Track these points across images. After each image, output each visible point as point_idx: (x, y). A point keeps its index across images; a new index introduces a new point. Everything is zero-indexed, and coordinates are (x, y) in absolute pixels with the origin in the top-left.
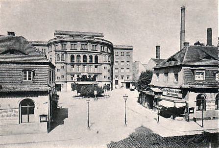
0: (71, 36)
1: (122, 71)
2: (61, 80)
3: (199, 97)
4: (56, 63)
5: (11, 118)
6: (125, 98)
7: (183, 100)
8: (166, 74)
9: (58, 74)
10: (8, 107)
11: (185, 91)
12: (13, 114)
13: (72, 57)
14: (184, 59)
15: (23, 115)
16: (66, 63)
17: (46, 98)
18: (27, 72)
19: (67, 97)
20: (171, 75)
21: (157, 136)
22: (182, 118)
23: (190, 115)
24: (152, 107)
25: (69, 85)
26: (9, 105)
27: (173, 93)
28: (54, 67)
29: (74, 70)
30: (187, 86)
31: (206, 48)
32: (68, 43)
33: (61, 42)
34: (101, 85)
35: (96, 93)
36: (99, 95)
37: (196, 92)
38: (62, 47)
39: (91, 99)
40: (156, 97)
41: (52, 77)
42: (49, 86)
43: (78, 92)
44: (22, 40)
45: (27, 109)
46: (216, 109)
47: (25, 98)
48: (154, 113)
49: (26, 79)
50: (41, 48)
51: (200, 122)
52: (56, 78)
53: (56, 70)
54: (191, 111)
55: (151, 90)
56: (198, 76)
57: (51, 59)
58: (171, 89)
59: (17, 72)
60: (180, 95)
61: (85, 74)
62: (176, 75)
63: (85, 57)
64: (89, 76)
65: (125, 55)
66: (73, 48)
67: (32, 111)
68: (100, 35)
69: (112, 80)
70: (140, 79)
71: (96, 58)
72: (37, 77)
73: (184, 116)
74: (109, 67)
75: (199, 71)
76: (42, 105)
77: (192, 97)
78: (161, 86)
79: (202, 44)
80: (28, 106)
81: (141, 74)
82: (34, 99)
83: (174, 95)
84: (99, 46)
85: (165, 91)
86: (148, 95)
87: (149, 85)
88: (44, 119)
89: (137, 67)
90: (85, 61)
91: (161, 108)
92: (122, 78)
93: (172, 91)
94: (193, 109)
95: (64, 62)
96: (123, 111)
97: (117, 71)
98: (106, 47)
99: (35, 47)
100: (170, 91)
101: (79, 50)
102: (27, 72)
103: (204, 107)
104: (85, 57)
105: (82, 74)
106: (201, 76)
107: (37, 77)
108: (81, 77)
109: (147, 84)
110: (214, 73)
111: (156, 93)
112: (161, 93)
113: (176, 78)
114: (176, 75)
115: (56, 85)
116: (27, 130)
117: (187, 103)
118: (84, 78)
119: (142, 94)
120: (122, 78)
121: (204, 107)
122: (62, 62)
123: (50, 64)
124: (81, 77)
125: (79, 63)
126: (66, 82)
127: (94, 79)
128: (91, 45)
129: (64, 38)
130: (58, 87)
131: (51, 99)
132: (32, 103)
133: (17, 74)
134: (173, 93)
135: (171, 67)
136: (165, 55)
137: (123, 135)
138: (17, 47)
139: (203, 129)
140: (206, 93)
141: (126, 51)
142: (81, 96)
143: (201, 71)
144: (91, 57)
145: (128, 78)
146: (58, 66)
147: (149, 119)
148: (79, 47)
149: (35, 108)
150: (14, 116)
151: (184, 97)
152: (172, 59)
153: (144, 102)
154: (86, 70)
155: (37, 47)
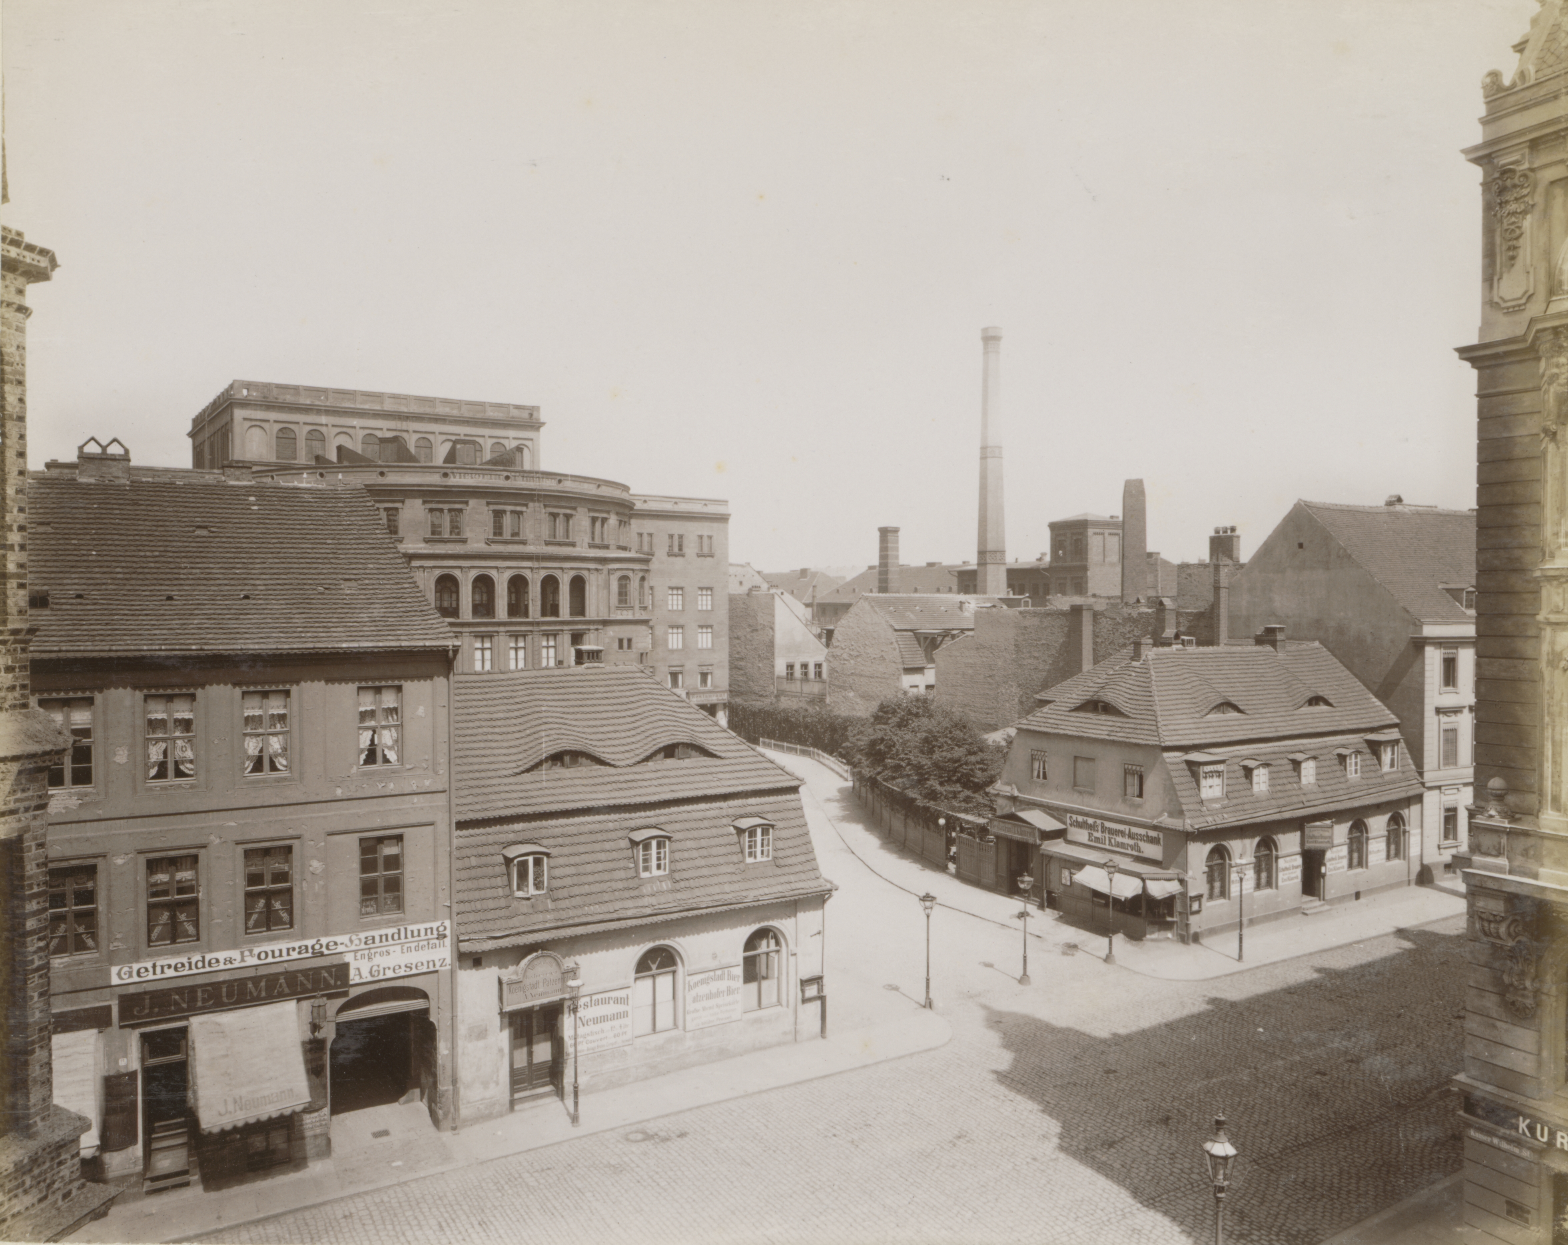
1: (675, 641)
7: (1172, 872)
10: (713, 964)
26: (715, 956)
56: (1210, 782)
58: (1108, 824)
65: (691, 549)
71: (578, 585)
83: (1122, 845)
93: (1112, 832)
94: (1199, 897)
100: (1104, 829)
103: (1269, 877)
117: (1182, 882)
121: (1269, 877)
134: (1120, 839)
144: (484, 584)
150: (730, 991)
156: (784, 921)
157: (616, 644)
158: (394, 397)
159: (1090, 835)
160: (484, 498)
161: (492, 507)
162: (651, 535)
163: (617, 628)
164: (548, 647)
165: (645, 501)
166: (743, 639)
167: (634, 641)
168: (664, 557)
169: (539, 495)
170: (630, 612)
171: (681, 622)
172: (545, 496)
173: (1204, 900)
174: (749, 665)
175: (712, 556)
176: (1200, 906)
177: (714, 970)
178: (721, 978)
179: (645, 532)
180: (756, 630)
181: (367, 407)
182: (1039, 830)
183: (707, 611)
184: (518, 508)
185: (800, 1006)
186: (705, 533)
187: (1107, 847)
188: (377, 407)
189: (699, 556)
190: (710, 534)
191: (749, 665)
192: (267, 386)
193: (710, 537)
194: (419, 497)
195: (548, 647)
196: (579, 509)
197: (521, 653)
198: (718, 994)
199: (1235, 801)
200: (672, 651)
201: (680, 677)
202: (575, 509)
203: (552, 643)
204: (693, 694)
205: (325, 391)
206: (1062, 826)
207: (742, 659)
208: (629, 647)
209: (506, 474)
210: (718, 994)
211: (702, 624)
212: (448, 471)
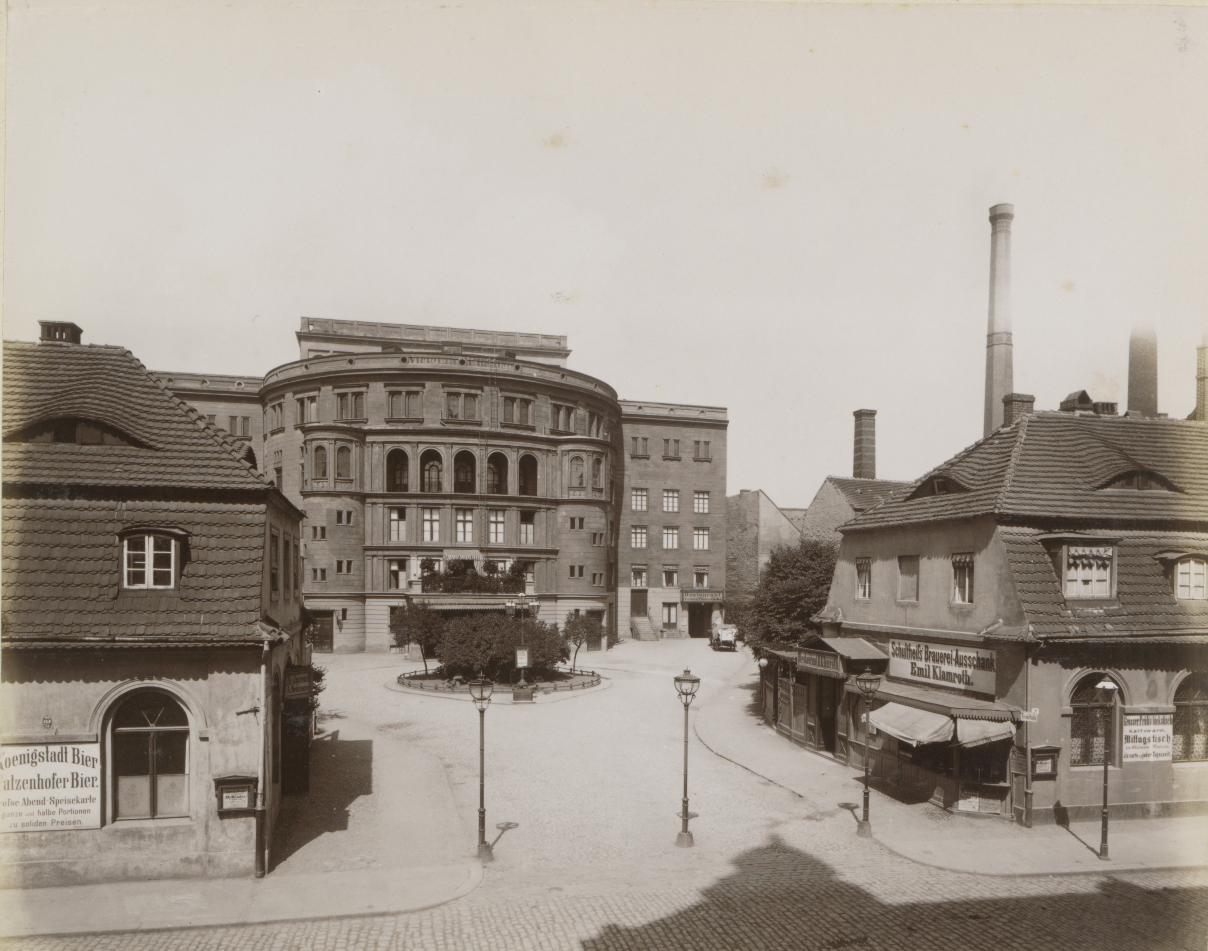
0: (391, 347)
1: (670, 541)
2: (336, 584)
3: (1084, 688)
4: (305, 495)
5: (59, 793)
6: (686, 686)
7: (999, 706)
8: (909, 562)
9: (317, 553)
11: (1007, 659)
12: (64, 770)
13: (397, 461)
14: (1007, 483)
15: (125, 782)
16: (362, 497)
17: (254, 685)
18: (149, 542)
19: (364, 687)
20: (937, 569)
21: (857, 897)
22: (994, 806)
23: (1037, 787)
24: (827, 738)
25: (379, 611)
27: (946, 668)
28: (295, 516)
29: (400, 533)
30: (1028, 631)
31: (1125, 426)
32: (372, 385)
33: (334, 379)
34: (555, 615)
35: (522, 659)
36: (543, 673)
37: (1067, 665)
38: (342, 407)
39: (500, 699)
40: (853, 685)
41: (283, 568)
42: (268, 620)
43: (1097, 735)
44: (119, 364)
45: (145, 744)
46: (1175, 760)
47: (136, 684)
48: (831, 778)
49: (138, 577)
50: (222, 411)
51: (1089, 831)
52: (308, 575)
53: (306, 530)
54: (1044, 767)
55: (818, 646)
56: (1080, 574)
57: (279, 470)
59: (93, 540)
60: (985, 681)
61: (466, 555)
62: (964, 570)
63: (465, 461)
64: (490, 567)
65: (687, 456)
66: (516, 420)
67: (169, 757)
68: (553, 344)
69: (612, 586)
70: (767, 584)
71: (528, 466)
72: (201, 569)
73: (1001, 794)
74: (596, 520)
75: (1087, 551)
76: (227, 724)
77: (1047, 696)
78: (883, 625)
79: (1110, 407)
80: (153, 728)
81: (774, 558)
82: (187, 690)
83: (948, 676)
84: (543, 406)
85: (902, 654)
86: (804, 677)
87: (815, 619)
88: (239, 800)
89: (749, 519)
90: (464, 485)
91: (877, 746)
92: (669, 581)
94: (1052, 753)
95: (353, 488)
96: (651, 754)
97: (639, 541)
98: (581, 412)
99: (195, 404)
101: (437, 426)
102: (149, 542)
103: (1109, 745)
104: (465, 461)
105: (451, 555)
106: (1095, 573)
107: (201, 569)
108: (440, 567)
109: (804, 616)
110: (1163, 561)
111: (854, 666)
112: (880, 667)
113: (962, 587)
114: (964, 570)
115: (309, 617)
116: (142, 858)
117: (1019, 724)
118: (460, 576)
119: (773, 674)
120: (669, 581)
121: (1109, 745)
122: (342, 487)
123: (271, 496)
124: (440, 567)
125: (430, 497)
126: (362, 598)
127: (515, 582)
128: (500, 396)
129: (350, 357)
130: (317, 628)
131: (275, 689)
132: (172, 709)
133: (91, 553)
134: (946, 668)
135: (942, 515)
136: (902, 463)
137: (674, 887)
138: (92, 406)
139: (1101, 866)
140: (1125, 673)
141: (691, 435)
142: (439, 675)
143: (1094, 551)
144: (498, 462)
145: (700, 577)
146: (319, 511)
147: (796, 799)
148: (432, 406)
149: (192, 744)
150: (76, 781)
151: (1003, 688)
152: (938, 483)
153: (786, 710)
154: (466, 533)
155: (203, 407)
156: (183, 683)
157: (568, 525)
158: (437, 330)
159: (914, 665)
160: (439, 381)
161: (446, 389)
162: (645, 439)
163: (568, 507)
164: (496, 523)
165: (640, 408)
166: (736, 540)
167: (585, 520)
168: (660, 461)
169: (493, 379)
170: (583, 493)
171: (676, 523)
172: (498, 379)
173: (1063, 760)
174: (740, 564)
175: (709, 461)
176: (1054, 766)
177: (47, 744)
178: (60, 758)
179: (640, 436)
180: (746, 529)
181: (411, 338)
182: (842, 657)
183: (704, 514)
184: (473, 391)
185: (215, 823)
186: (702, 439)
187: (931, 681)
188: (420, 338)
189: (696, 460)
190: (707, 440)
191: (740, 564)
192: (326, 321)
193: (707, 443)
194: (381, 381)
195: (496, 523)
196: (539, 396)
197: (469, 526)
198: (54, 782)
199: (1133, 609)
200: (667, 550)
201: (675, 575)
202: (534, 394)
203: (500, 519)
204: (687, 592)
205: (374, 325)
206: (885, 657)
207: (735, 559)
208: (581, 526)
209: (460, 358)
210: (54, 782)
211: (698, 526)
212: (407, 356)
